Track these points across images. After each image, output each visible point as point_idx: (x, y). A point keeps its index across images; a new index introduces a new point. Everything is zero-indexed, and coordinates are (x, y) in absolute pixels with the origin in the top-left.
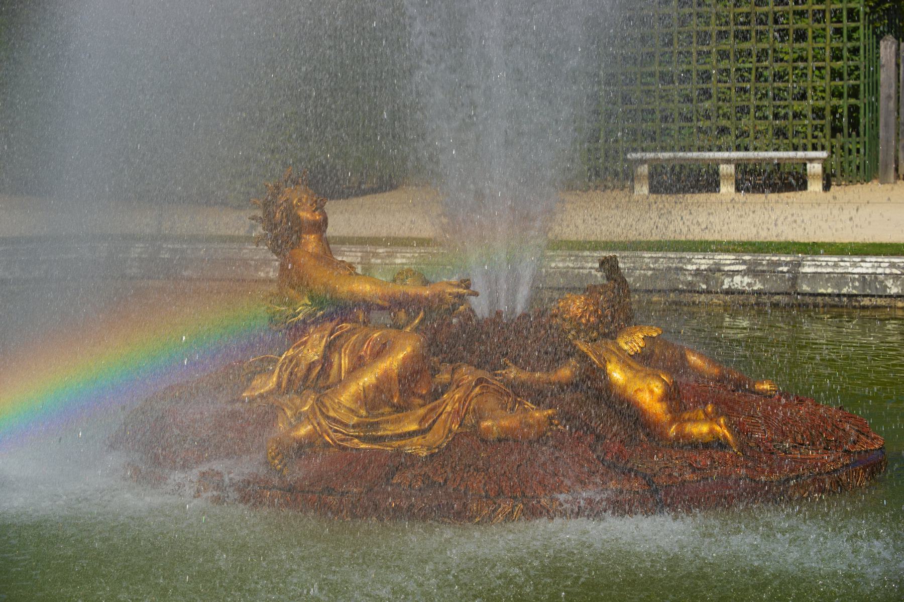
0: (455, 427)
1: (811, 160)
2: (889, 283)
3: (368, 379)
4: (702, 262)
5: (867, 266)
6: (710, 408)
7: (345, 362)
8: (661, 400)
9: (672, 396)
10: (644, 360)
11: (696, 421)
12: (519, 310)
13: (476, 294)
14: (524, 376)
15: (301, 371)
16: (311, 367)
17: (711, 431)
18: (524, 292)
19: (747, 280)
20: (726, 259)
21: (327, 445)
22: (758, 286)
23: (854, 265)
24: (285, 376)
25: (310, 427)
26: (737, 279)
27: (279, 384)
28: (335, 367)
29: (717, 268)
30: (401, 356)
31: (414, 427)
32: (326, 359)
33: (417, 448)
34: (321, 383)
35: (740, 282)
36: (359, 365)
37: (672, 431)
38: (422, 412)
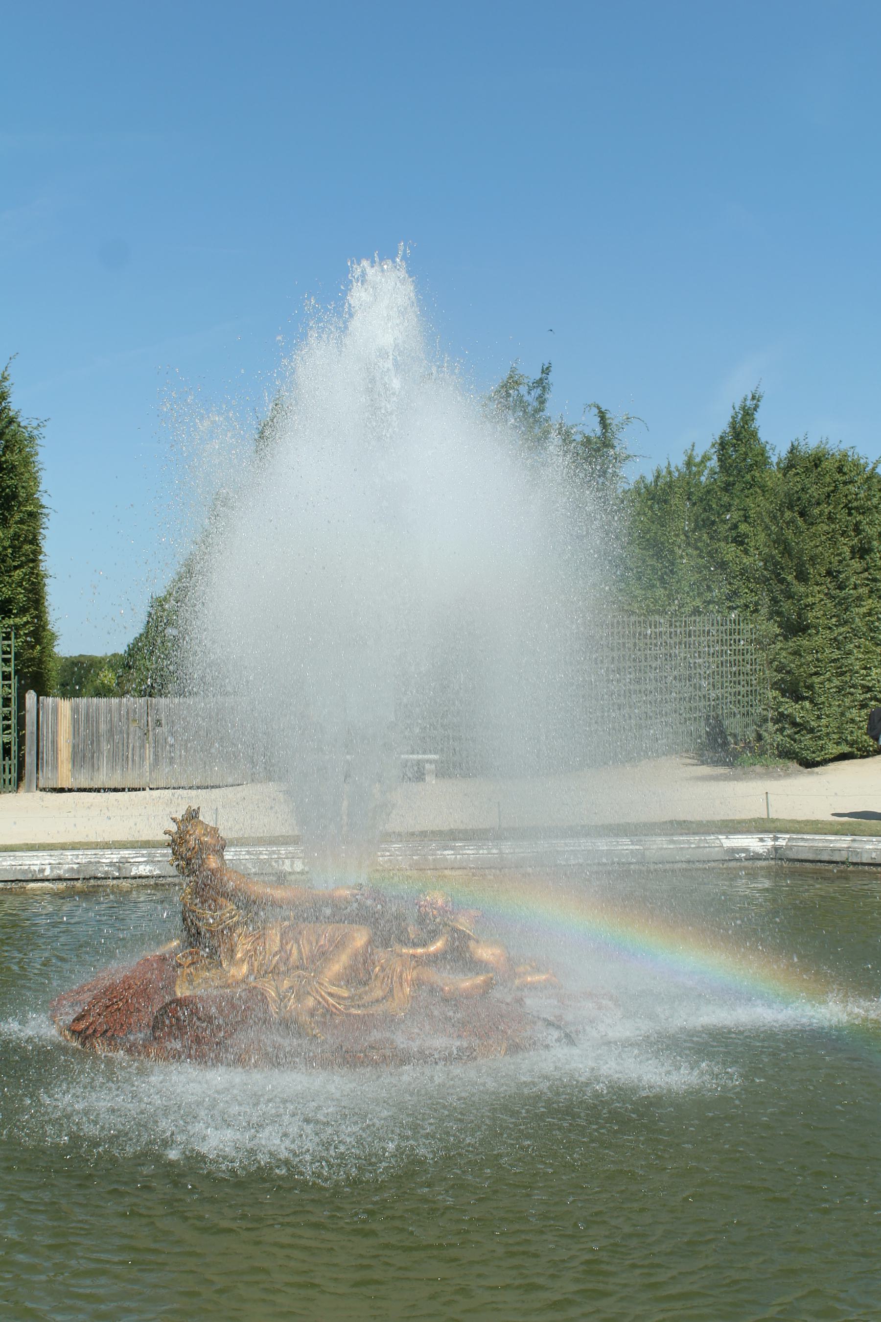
2: (249, 866)
19: (148, 868)
26: (141, 867)
29: (124, 861)
35: (144, 870)
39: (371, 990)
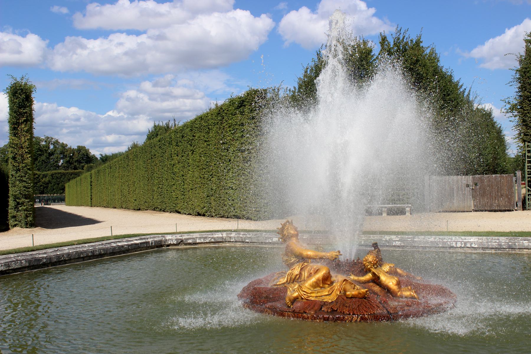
0: (338, 293)
1: (407, 207)
3: (313, 279)
4: (387, 238)
5: (432, 239)
6: (409, 288)
7: (306, 274)
8: (396, 285)
9: (399, 284)
10: (392, 273)
11: (406, 291)
12: (353, 258)
13: (341, 255)
14: (356, 278)
15: (293, 277)
16: (297, 275)
17: (410, 294)
18: (353, 254)
20: (394, 237)
21: (302, 299)
22: (402, 244)
23: (429, 238)
24: (289, 278)
25: (297, 293)
27: (287, 281)
28: (303, 276)
30: (322, 273)
31: (327, 293)
32: (300, 274)
33: (329, 299)
34: (299, 280)
35: (398, 243)
36: (310, 275)
37: (399, 294)
38: (329, 289)
39: (322, 291)
